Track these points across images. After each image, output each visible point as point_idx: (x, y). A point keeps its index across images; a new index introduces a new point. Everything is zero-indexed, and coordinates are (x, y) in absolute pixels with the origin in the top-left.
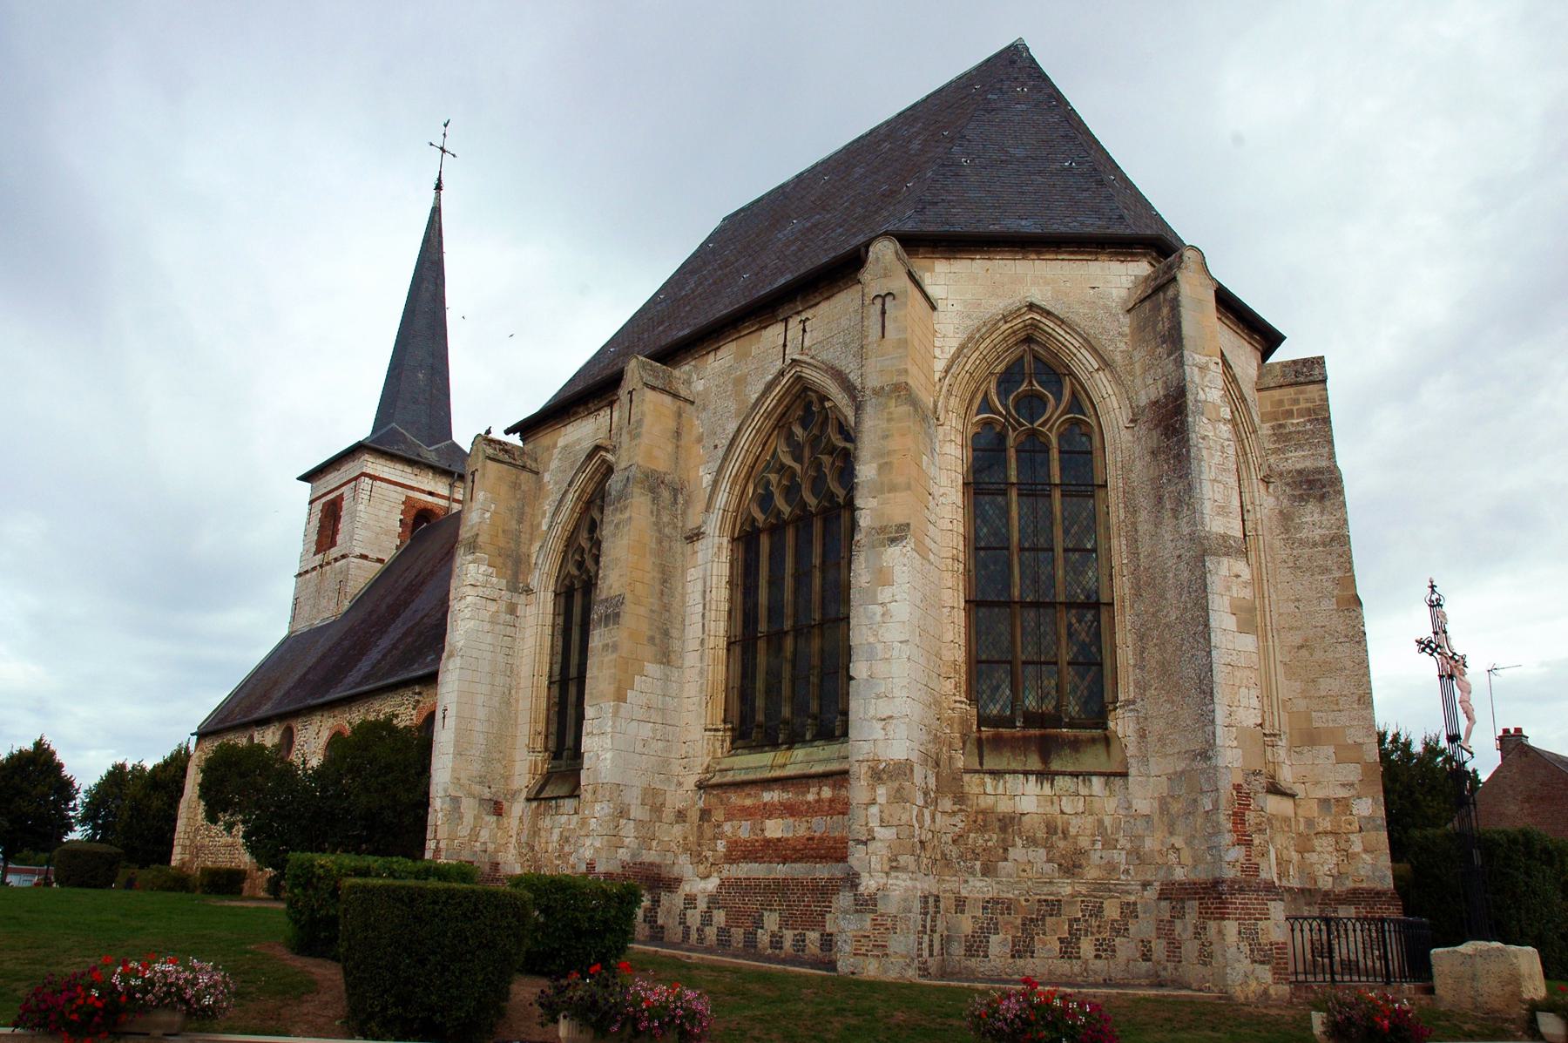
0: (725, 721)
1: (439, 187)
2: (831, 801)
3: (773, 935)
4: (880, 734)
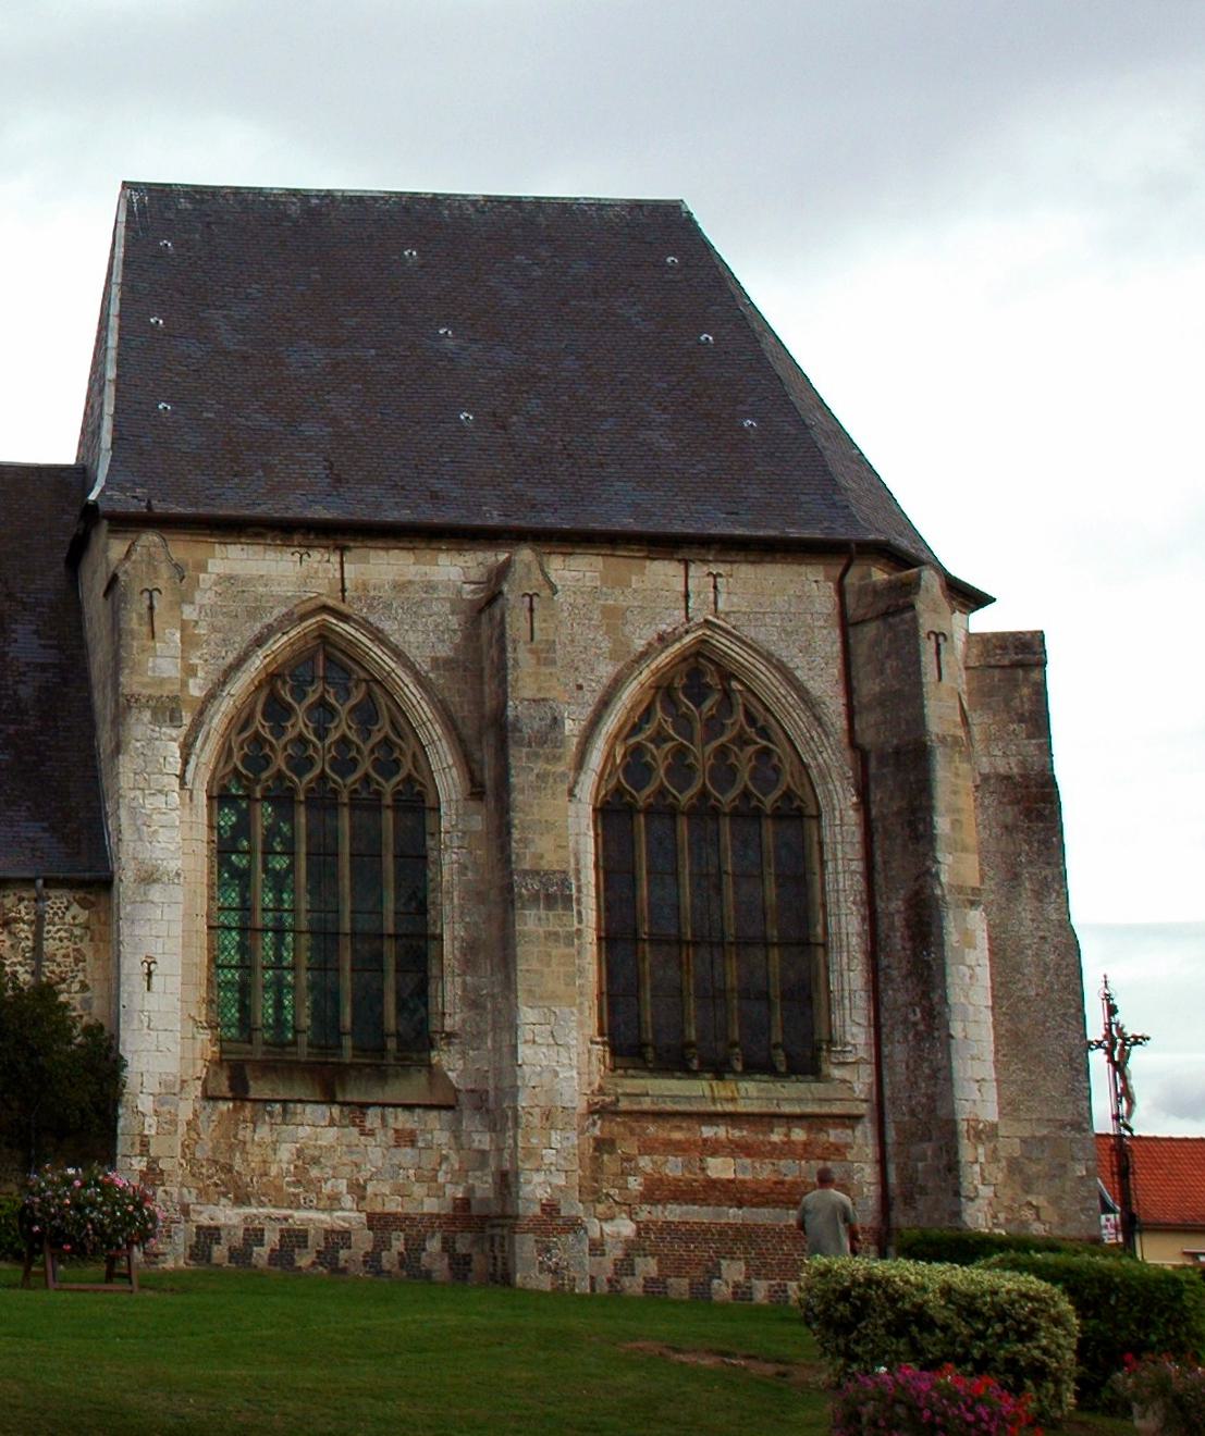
0: (601, 1034)
2: (806, 1145)
3: (737, 1285)
4: (977, 1096)
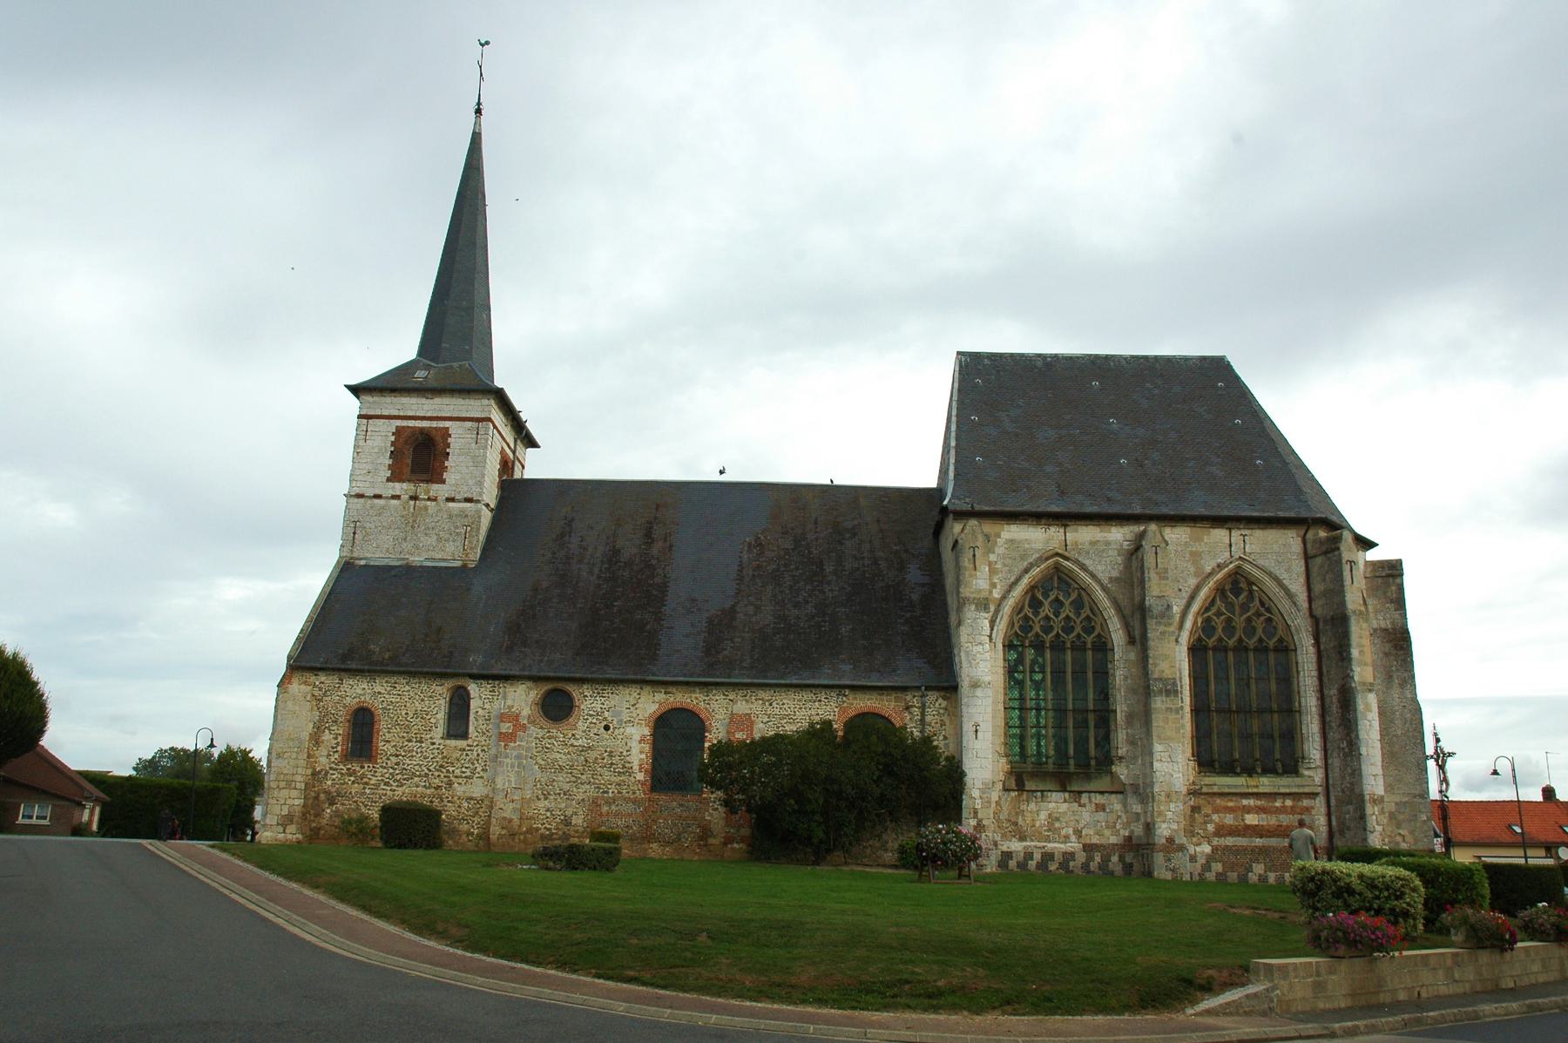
1: (478, 112)
